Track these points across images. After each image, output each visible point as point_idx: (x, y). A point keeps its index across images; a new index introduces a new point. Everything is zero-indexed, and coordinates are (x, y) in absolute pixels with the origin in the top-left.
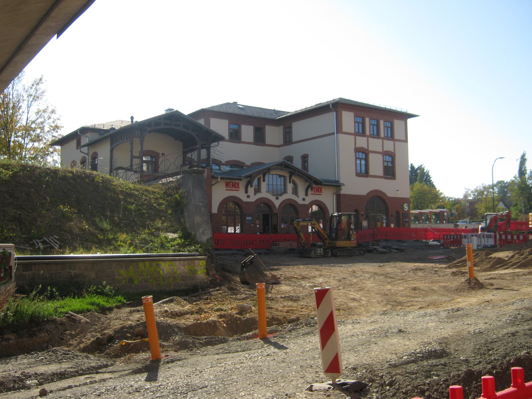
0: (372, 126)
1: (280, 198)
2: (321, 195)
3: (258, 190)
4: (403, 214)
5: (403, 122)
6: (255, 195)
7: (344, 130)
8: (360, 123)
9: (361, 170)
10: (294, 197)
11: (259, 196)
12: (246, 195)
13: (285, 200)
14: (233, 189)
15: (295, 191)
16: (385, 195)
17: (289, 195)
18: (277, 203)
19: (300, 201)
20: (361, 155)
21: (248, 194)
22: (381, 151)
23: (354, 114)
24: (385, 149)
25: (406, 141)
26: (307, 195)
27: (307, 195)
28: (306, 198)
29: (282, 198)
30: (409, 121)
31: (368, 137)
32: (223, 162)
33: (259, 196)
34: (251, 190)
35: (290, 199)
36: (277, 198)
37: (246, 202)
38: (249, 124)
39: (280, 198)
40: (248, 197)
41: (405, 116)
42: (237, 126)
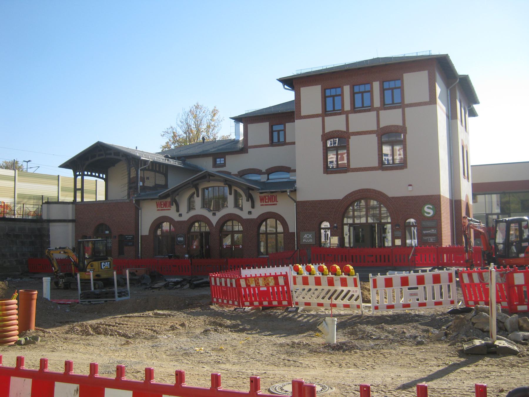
1: (217, 213)
3: (191, 207)
7: (302, 114)
10: (237, 212)
11: (193, 213)
12: (178, 214)
13: (222, 217)
14: (165, 208)
17: (230, 209)
21: (180, 213)
22: (375, 128)
26: (253, 207)
27: (253, 207)
29: (220, 214)
32: (264, 171)
34: (184, 207)
35: (231, 214)
36: (214, 214)
39: (217, 213)
40: (180, 215)
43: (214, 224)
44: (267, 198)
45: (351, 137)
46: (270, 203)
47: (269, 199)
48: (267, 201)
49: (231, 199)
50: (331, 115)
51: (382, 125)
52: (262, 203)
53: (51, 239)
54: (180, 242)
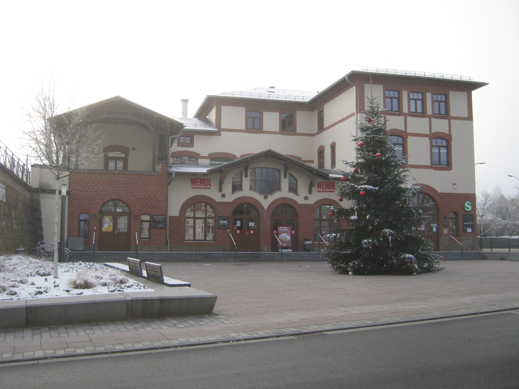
0: (436, 104)
1: (269, 197)
3: (236, 188)
4: (463, 215)
5: (464, 94)
6: (232, 193)
9: (440, 161)
10: (292, 196)
11: (238, 194)
12: (220, 194)
13: (275, 200)
15: (293, 189)
16: (434, 191)
17: (284, 193)
18: (266, 203)
19: (300, 200)
20: (439, 142)
21: (223, 192)
23: (384, 88)
24: (433, 131)
25: (470, 117)
26: (310, 192)
27: (310, 192)
28: (309, 196)
29: (272, 198)
30: (475, 94)
31: (405, 115)
33: (238, 194)
34: (227, 188)
36: (266, 197)
37: (220, 203)
38: (273, 111)
39: (269, 197)
40: (223, 196)
41: (468, 87)
43: (266, 209)
47: (326, 185)
49: (285, 183)
51: (433, 131)
52: (319, 190)
53: (43, 216)
54: (224, 225)
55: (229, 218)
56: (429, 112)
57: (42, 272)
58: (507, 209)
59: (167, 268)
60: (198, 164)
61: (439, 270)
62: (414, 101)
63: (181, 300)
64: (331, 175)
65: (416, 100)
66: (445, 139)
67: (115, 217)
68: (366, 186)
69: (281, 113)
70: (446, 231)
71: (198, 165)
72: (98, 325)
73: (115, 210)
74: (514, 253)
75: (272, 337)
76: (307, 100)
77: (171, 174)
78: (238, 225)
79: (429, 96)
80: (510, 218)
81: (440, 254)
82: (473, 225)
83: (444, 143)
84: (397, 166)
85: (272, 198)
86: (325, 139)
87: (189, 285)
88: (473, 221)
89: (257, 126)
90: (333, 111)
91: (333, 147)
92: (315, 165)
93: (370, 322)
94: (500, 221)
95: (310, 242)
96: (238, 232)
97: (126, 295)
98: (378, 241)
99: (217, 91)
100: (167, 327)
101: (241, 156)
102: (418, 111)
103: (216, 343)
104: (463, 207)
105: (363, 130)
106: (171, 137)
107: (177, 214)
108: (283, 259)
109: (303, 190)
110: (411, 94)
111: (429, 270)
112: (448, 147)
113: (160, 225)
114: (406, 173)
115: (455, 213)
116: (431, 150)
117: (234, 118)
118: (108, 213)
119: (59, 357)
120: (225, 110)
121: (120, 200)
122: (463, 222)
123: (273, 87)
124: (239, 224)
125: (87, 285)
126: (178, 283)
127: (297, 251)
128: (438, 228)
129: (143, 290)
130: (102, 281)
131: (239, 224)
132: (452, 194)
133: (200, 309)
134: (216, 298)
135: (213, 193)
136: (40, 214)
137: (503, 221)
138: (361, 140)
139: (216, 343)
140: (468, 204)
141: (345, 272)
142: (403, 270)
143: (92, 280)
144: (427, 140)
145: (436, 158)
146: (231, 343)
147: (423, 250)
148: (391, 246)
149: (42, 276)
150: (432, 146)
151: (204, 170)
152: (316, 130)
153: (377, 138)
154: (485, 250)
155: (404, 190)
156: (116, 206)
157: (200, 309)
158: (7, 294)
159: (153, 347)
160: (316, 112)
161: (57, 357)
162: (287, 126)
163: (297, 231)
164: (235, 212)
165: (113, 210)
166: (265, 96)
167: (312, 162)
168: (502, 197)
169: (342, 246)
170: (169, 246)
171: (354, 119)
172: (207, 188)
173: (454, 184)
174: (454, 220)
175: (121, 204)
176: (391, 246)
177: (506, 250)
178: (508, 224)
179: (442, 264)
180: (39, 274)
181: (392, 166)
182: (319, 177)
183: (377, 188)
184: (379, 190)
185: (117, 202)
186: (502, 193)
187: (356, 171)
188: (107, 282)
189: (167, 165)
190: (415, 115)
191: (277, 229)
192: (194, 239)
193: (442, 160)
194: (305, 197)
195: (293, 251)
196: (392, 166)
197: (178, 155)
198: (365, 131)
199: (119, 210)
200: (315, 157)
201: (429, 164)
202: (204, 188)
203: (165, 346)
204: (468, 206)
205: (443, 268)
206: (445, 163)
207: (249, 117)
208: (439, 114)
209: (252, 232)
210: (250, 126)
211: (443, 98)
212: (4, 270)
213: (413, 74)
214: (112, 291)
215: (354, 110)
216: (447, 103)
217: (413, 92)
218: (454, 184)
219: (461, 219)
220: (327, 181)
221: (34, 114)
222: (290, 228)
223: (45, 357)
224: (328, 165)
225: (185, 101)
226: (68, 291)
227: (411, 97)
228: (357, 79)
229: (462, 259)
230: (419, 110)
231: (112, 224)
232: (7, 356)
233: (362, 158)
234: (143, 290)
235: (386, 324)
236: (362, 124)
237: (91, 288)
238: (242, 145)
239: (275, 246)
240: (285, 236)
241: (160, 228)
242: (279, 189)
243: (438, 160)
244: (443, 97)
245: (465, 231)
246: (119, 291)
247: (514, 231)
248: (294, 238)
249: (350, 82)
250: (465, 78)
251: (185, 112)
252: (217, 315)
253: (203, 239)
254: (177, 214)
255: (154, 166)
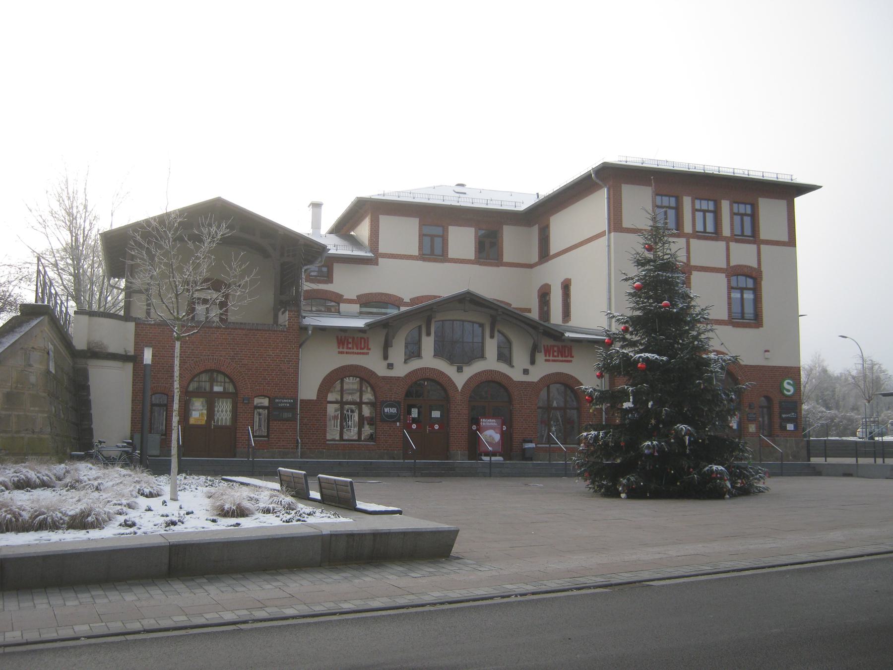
0: (737, 219)
1: (465, 369)
2: (570, 361)
3: (413, 352)
5: (782, 204)
6: (406, 362)
7: (624, 225)
8: (746, 215)
9: (743, 313)
10: (503, 368)
11: (415, 364)
12: (385, 363)
13: (476, 375)
15: (505, 356)
17: (490, 363)
18: (460, 379)
19: (516, 375)
20: (742, 281)
21: (390, 361)
22: (723, 265)
25: (791, 242)
26: (533, 362)
27: (533, 362)
29: (470, 371)
30: (799, 201)
32: (407, 300)
33: (415, 364)
34: (397, 353)
35: (491, 371)
36: (460, 370)
37: (384, 378)
40: (390, 366)
41: (788, 191)
42: (441, 229)
43: (460, 388)
44: (556, 349)
45: (693, 272)
46: (561, 358)
48: (556, 354)
49: (491, 347)
50: (699, 238)
51: (732, 264)
54: (391, 416)
55: (399, 403)
56: (726, 231)
57: (147, 491)
58: (833, 391)
59: (362, 486)
60: (339, 312)
61: (760, 492)
62: (739, 217)
63: (404, 534)
64: (567, 334)
65: (704, 212)
66: (751, 277)
67: (211, 400)
68: (647, 355)
69: (478, 229)
70: (752, 428)
71: (339, 313)
72: (143, 585)
73: (212, 387)
74: (862, 465)
75: (571, 589)
76: (522, 207)
77: (305, 329)
78: (413, 416)
79: (725, 205)
80: (837, 407)
81: (763, 465)
82: (796, 418)
83: (750, 283)
84: (695, 321)
85: (470, 371)
86: (553, 274)
87: (400, 512)
88: (796, 413)
89: (438, 251)
90: (564, 228)
91: (566, 287)
92: (535, 315)
93: (708, 568)
94: (822, 412)
95: (532, 445)
96: (414, 426)
97: (311, 526)
98: (668, 443)
99: (372, 191)
100: (395, 577)
101: (414, 301)
102: (708, 230)
103: (492, 598)
104: (781, 389)
105: (640, 263)
106: (306, 267)
107: (314, 397)
108: (491, 472)
109: (520, 357)
110: (697, 202)
111: (745, 492)
112: (756, 290)
113: (286, 415)
114: (710, 335)
115: (768, 398)
116: (729, 294)
117: (401, 236)
118: (198, 394)
119: (261, 621)
120: (385, 221)
121: (219, 372)
122: (780, 414)
123: (462, 185)
124: (415, 413)
125: (241, 512)
126: (382, 508)
127: (510, 459)
128: (740, 424)
129: (326, 520)
130: (262, 505)
131: (415, 413)
132: (763, 367)
133: (434, 548)
134: (455, 533)
135: (373, 362)
136: (89, 394)
137: (829, 413)
138: (638, 281)
139: (492, 598)
140: (788, 383)
141: (611, 493)
142: (708, 491)
143: (246, 504)
144: (722, 277)
145: (736, 309)
146: (513, 599)
147: (737, 459)
148: (688, 451)
149: (147, 496)
150: (730, 288)
151: (360, 323)
152: (535, 258)
153: (662, 276)
154: (814, 460)
155: (707, 362)
156: (212, 381)
157: (434, 548)
158: (120, 525)
159: (393, 605)
160: (535, 230)
161: (27, 643)
162: (488, 249)
163: (510, 427)
164: (408, 394)
165: (208, 389)
166: (452, 200)
167: (529, 311)
168: (825, 371)
169: (606, 450)
170: (299, 450)
171: (603, 241)
172: (363, 353)
173: (766, 351)
174: (765, 410)
175: (221, 378)
176: (688, 451)
177: (851, 461)
178: (837, 416)
179: (773, 484)
180: (142, 494)
181: (687, 323)
182: (548, 338)
183: (665, 358)
184: (668, 362)
185: (215, 375)
186: (825, 364)
187: (626, 330)
188: (271, 506)
189: (299, 316)
190: (702, 236)
191: (477, 423)
192: (341, 439)
193: (746, 311)
194: (525, 369)
195: (505, 460)
196: (687, 323)
197: (313, 296)
198: (643, 265)
199: (217, 389)
200: (534, 305)
201: (725, 317)
202: (358, 353)
203: (361, 608)
204: (788, 387)
205: (767, 489)
206: (752, 316)
207: (424, 235)
208: (742, 235)
209: (436, 427)
210: (427, 251)
211: (749, 210)
212: (84, 487)
213: (700, 170)
214: (287, 522)
215: (605, 228)
216: (754, 217)
217: (701, 199)
218: (766, 351)
219: (776, 409)
220: (560, 344)
221: (51, 221)
222: (500, 421)
223: (75, 636)
224: (556, 317)
225: (316, 206)
226: (214, 521)
227: (697, 207)
228: (612, 177)
229: (781, 474)
230: (710, 228)
231: (205, 412)
232: (13, 636)
233: (639, 309)
234: (334, 520)
235: (734, 571)
236: (638, 253)
237: (247, 516)
238: (413, 280)
239: (474, 448)
240: (491, 434)
241: (287, 420)
242: (482, 357)
243: (739, 311)
244: (749, 207)
245: (784, 428)
246: (299, 520)
247: (845, 429)
248: (507, 437)
249: (598, 181)
250: (784, 178)
251: (316, 223)
252: (458, 558)
253: (356, 437)
254: (314, 397)
255: (276, 317)
